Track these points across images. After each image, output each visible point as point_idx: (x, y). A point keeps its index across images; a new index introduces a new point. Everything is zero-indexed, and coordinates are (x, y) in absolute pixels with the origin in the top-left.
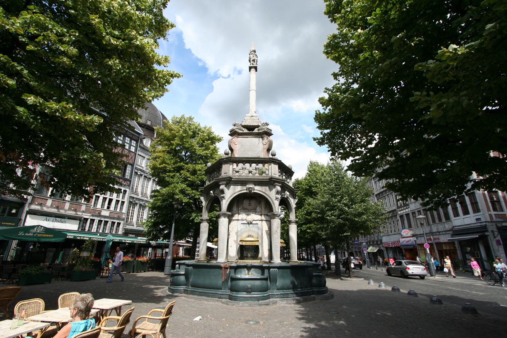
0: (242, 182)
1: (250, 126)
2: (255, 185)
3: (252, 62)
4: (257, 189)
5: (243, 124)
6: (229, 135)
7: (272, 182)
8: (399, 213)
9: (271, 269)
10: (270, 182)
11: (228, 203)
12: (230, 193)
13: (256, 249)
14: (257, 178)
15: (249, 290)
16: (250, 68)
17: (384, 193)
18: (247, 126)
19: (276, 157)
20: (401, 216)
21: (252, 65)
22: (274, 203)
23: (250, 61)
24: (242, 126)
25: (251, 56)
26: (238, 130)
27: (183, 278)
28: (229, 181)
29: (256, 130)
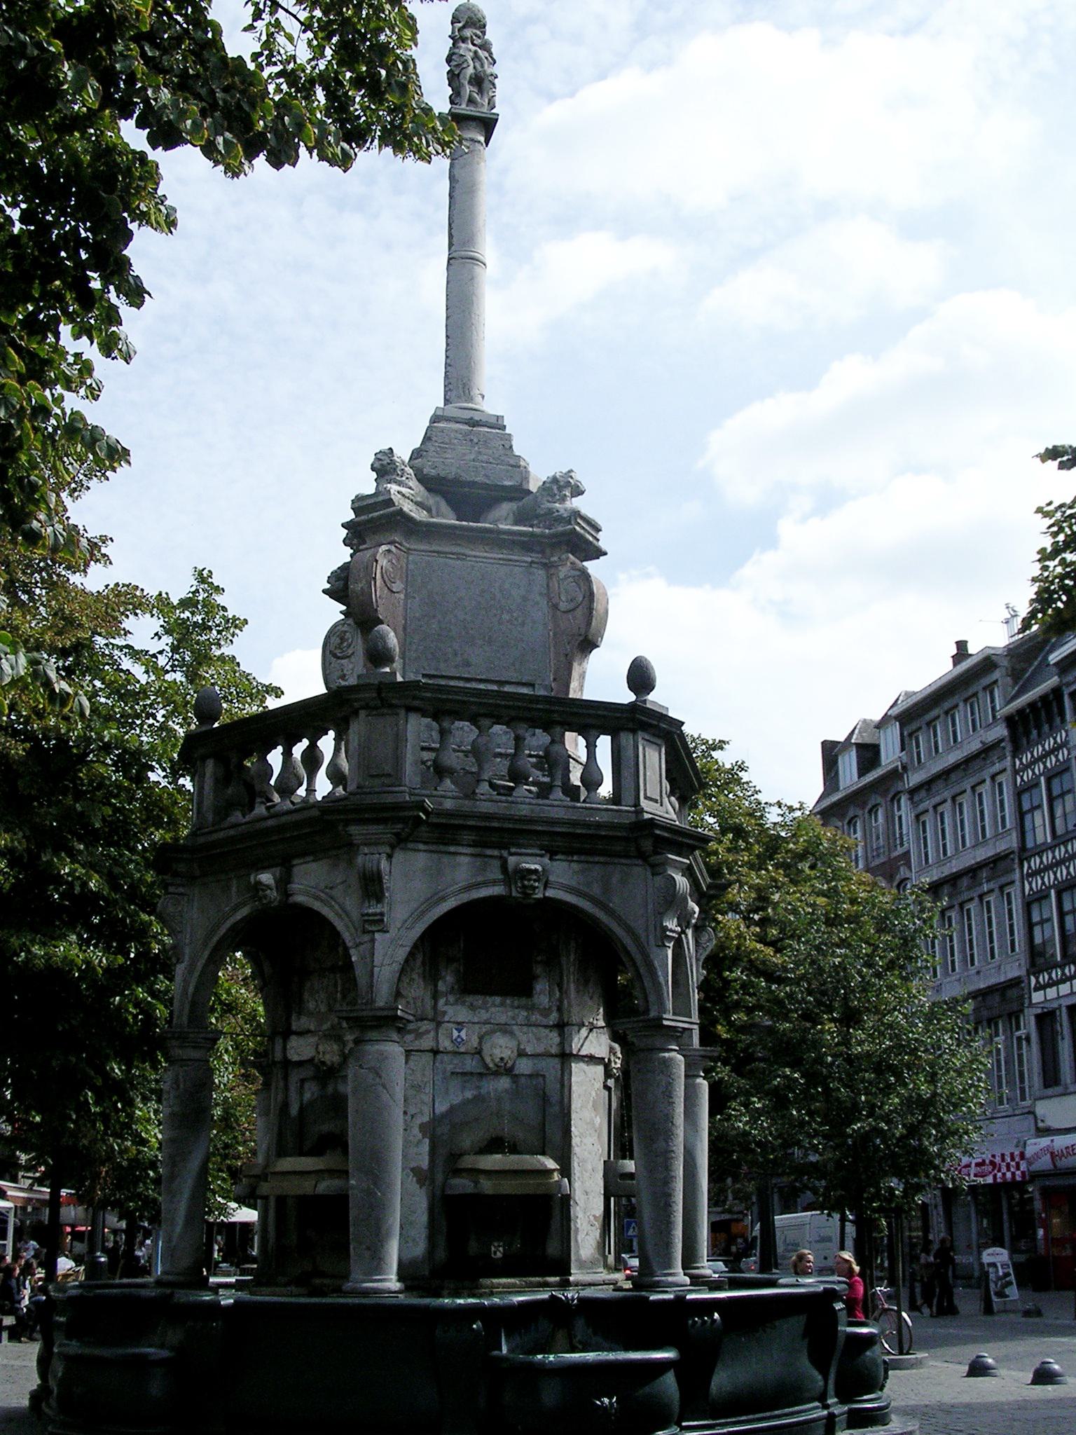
0: (496, 835)
2: (552, 853)
3: (468, 89)
4: (561, 879)
8: (1037, 997)
17: (965, 882)
18: (457, 482)
19: (656, 698)
20: (1046, 1019)
21: (463, 108)
26: (407, 507)
29: (502, 519)
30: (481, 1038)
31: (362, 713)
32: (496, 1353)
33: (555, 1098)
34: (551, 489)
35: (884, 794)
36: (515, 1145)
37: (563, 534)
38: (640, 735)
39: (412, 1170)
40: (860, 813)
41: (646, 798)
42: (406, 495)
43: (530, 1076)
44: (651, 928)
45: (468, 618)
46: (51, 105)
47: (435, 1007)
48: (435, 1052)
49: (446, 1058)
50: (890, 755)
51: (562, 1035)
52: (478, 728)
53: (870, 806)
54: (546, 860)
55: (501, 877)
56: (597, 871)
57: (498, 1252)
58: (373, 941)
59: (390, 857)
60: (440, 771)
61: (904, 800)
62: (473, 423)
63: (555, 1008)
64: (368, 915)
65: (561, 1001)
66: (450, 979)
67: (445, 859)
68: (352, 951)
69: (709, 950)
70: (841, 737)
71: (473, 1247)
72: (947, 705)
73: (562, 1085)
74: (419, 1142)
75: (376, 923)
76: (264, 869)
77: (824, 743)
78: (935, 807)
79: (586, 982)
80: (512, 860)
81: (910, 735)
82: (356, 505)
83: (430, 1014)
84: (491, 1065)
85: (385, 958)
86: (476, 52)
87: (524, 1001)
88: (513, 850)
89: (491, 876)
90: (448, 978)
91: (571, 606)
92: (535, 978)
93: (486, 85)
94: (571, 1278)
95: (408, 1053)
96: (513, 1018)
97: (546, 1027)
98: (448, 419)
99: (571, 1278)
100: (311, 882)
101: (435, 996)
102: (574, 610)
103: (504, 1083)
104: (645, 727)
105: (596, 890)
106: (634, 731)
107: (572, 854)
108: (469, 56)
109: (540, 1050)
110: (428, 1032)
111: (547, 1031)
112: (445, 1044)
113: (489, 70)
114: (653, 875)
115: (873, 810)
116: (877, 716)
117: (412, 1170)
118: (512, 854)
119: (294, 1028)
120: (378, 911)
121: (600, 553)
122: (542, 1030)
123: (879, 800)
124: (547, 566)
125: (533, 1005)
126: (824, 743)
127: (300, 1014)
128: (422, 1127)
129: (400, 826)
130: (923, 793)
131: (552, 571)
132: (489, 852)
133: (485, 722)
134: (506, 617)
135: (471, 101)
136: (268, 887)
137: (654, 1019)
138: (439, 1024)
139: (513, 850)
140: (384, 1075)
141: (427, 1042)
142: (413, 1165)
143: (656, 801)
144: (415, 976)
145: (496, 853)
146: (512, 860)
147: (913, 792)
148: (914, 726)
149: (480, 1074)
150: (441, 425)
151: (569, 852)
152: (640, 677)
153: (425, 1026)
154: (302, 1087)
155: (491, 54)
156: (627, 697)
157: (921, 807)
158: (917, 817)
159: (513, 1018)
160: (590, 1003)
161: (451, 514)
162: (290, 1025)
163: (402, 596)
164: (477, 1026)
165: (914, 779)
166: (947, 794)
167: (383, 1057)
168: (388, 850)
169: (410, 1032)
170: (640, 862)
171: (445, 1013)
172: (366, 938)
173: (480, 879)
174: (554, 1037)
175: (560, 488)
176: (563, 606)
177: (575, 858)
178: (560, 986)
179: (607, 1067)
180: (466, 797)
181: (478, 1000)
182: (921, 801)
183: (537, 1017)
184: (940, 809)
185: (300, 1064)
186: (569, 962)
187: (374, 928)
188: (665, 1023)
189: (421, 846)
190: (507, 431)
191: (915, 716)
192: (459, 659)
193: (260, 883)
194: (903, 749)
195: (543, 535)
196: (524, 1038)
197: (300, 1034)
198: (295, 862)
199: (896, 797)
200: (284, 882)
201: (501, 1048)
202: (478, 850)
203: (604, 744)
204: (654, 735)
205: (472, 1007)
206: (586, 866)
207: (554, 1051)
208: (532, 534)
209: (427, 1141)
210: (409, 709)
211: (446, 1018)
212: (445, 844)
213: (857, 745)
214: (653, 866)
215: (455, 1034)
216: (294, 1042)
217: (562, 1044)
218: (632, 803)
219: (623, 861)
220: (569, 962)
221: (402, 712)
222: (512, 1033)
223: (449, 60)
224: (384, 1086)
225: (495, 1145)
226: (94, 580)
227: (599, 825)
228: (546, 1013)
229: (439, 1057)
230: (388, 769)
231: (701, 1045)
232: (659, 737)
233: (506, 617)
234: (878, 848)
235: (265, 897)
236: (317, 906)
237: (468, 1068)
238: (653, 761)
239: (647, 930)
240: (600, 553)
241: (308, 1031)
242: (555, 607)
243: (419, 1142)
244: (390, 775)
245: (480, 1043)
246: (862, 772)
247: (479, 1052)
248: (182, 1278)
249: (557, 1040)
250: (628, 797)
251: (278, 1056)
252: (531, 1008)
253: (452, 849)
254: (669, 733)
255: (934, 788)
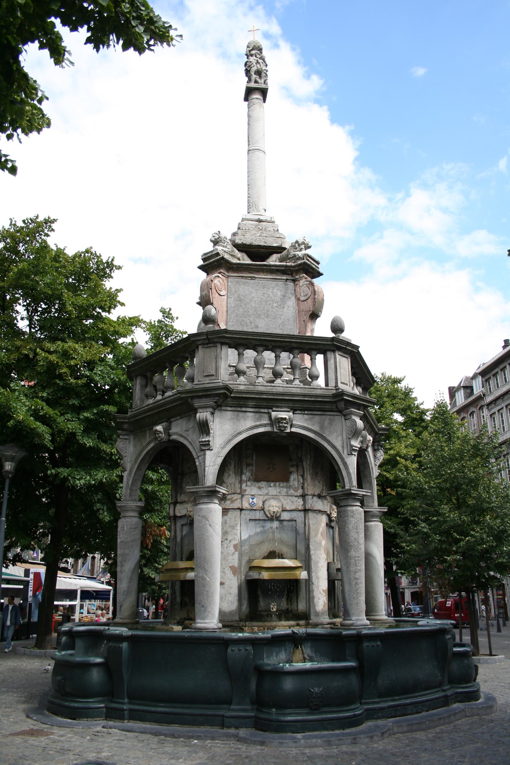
0: (263, 402)
1: (259, 247)
2: (294, 410)
3: (254, 77)
4: (300, 424)
5: (238, 241)
6: (201, 268)
7: (342, 405)
9: (366, 644)
10: (334, 404)
11: (220, 461)
12: (226, 431)
13: (291, 588)
14: (280, 390)
15: (303, 701)
16: (249, 92)
18: (251, 246)
19: (345, 335)
21: (252, 85)
22: (345, 464)
23: (248, 72)
24: (236, 246)
25: (252, 59)
26: (227, 256)
27: (96, 676)
28: (226, 399)
29: (273, 260)
30: (264, 502)
31: (200, 347)
32: (262, 662)
33: (301, 530)
34: (295, 246)
35: (476, 407)
36: (282, 555)
37: (300, 265)
38: (337, 354)
39: (230, 567)
40: (466, 415)
41: (342, 383)
42: (225, 251)
43: (289, 521)
44: (345, 446)
45: (257, 306)
46: (372, 385)
47: (241, 488)
48: (241, 510)
49: (246, 512)
50: (478, 388)
51: (304, 500)
52: (257, 352)
53: (470, 413)
54: (291, 414)
55: (269, 422)
56: (317, 418)
57: (274, 608)
58: (205, 454)
59: (213, 414)
60: (239, 372)
61: (485, 410)
62: (260, 221)
63: (300, 488)
64: (202, 442)
65: (303, 483)
66: (248, 474)
67: (241, 414)
68: (196, 460)
69: (381, 460)
70: (456, 385)
71: (262, 604)
72: (501, 367)
73: (305, 524)
74: (233, 554)
75: (206, 446)
76: (158, 424)
77: (449, 388)
78: (498, 411)
79: (316, 474)
80: (274, 414)
81: (486, 381)
82: (203, 257)
83: (239, 491)
84: (269, 515)
85: (211, 463)
86: (257, 60)
87: (285, 484)
88: (274, 409)
89: (265, 422)
90: (247, 474)
91: (306, 298)
92: (291, 473)
93: (263, 75)
94: (310, 622)
95: (225, 511)
96: (280, 492)
97: (296, 496)
98: (248, 220)
99: (310, 622)
100: (180, 430)
101: (241, 482)
102: (307, 299)
103: (276, 524)
104: (339, 349)
105: (316, 428)
106: (334, 351)
107: (304, 410)
108: (254, 62)
109: (293, 507)
110: (237, 499)
111: (297, 498)
112: (246, 505)
113: (264, 68)
114: (345, 420)
115: (472, 414)
116: (471, 375)
117: (230, 567)
118: (273, 411)
119: (179, 500)
120: (207, 439)
121: (320, 274)
122: (294, 497)
123: (474, 409)
124: (294, 281)
125: (290, 486)
126: (449, 388)
127: (181, 494)
128: (235, 546)
129: (217, 398)
130: (493, 405)
131: (297, 283)
132: (262, 410)
133: (261, 349)
134: (275, 305)
135: (256, 82)
136: (160, 432)
137: (347, 490)
138: (243, 496)
139: (274, 409)
140: (210, 520)
141: (237, 505)
142: (231, 565)
143: (347, 384)
144: (231, 473)
145: (266, 411)
146: (274, 414)
147: (488, 405)
148: (487, 377)
149: (264, 520)
150: (245, 222)
151: (303, 410)
152: (337, 328)
153: (235, 497)
154: (182, 528)
155: (265, 62)
156: (331, 335)
157: (492, 411)
158: (491, 416)
159: (280, 492)
160: (318, 484)
161: (249, 259)
162: (177, 499)
163: (226, 297)
164: (261, 497)
165: (489, 399)
166: (503, 405)
167: (210, 511)
168: (211, 410)
169: (229, 499)
170: (339, 414)
171: (245, 490)
172: (202, 453)
173: (258, 423)
174: (300, 502)
175: (299, 245)
176: (302, 298)
177: (306, 412)
178: (303, 476)
179: (329, 516)
180: (251, 384)
181: (263, 484)
182: (492, 408)
183: (292, 492)
184: (501, 412)
185: (181, 517)
186: (307, 464)
187: (205, 448)
188: (353, 492)
189: (229, 408)
190: (276, 223)
191: (488, 372)
192: (253, 325)
193: (156, 430)
194: (483, 387)
195: (291, 266)
196: (284, 502)
197: (181, 503)
198: (172, 420)
199: (481, 408)
200: (167, 430)
201: (274, 506)
202: (257, 410)
203: (320, 358)
204: (344, 353)
205: (260, 488)
206: (311, 416)
207: (300, 508)
208: (286, 266)
209: (237, 553)
210: (222, 344)
211: (246, 493)
212: (241, 407)
213: (463, 387)
214: (344, 416)
215: (251, 500)
216: (178, 507)
217: (304, 504)
218: (334, 385)
219: (330, 413)
220: (307, 464)
221: (219, 345)
222: (279, 499)
223: (246, 65)
224: (210, 525)
225: (272, 555)
226: (114, 315)
227: (317, 396)
228: (296, 490)
229: (243, 512)
230: (213, 372)
231: (379, 506)
232: (347, 354)
233: (275, 305)
234: (475, 430)
235: (159, 437)
236: (182, 440)
237: (257, 517)
238: (344, 364)
239: (343, 447)
240: (320, 274)
241: (185, 502)
242: (298, 299)
243: (233, 554)
244: (213, 375)
245: (263, 505)
246: (466, 397)
247: (263, 509)
248: (125, 621)
249: (302, 503)
250: (332, 384)
251: (172, 514)
252: (289, 487)
253: (244, 409)
254: (352, 351)
255: (498, 403)
